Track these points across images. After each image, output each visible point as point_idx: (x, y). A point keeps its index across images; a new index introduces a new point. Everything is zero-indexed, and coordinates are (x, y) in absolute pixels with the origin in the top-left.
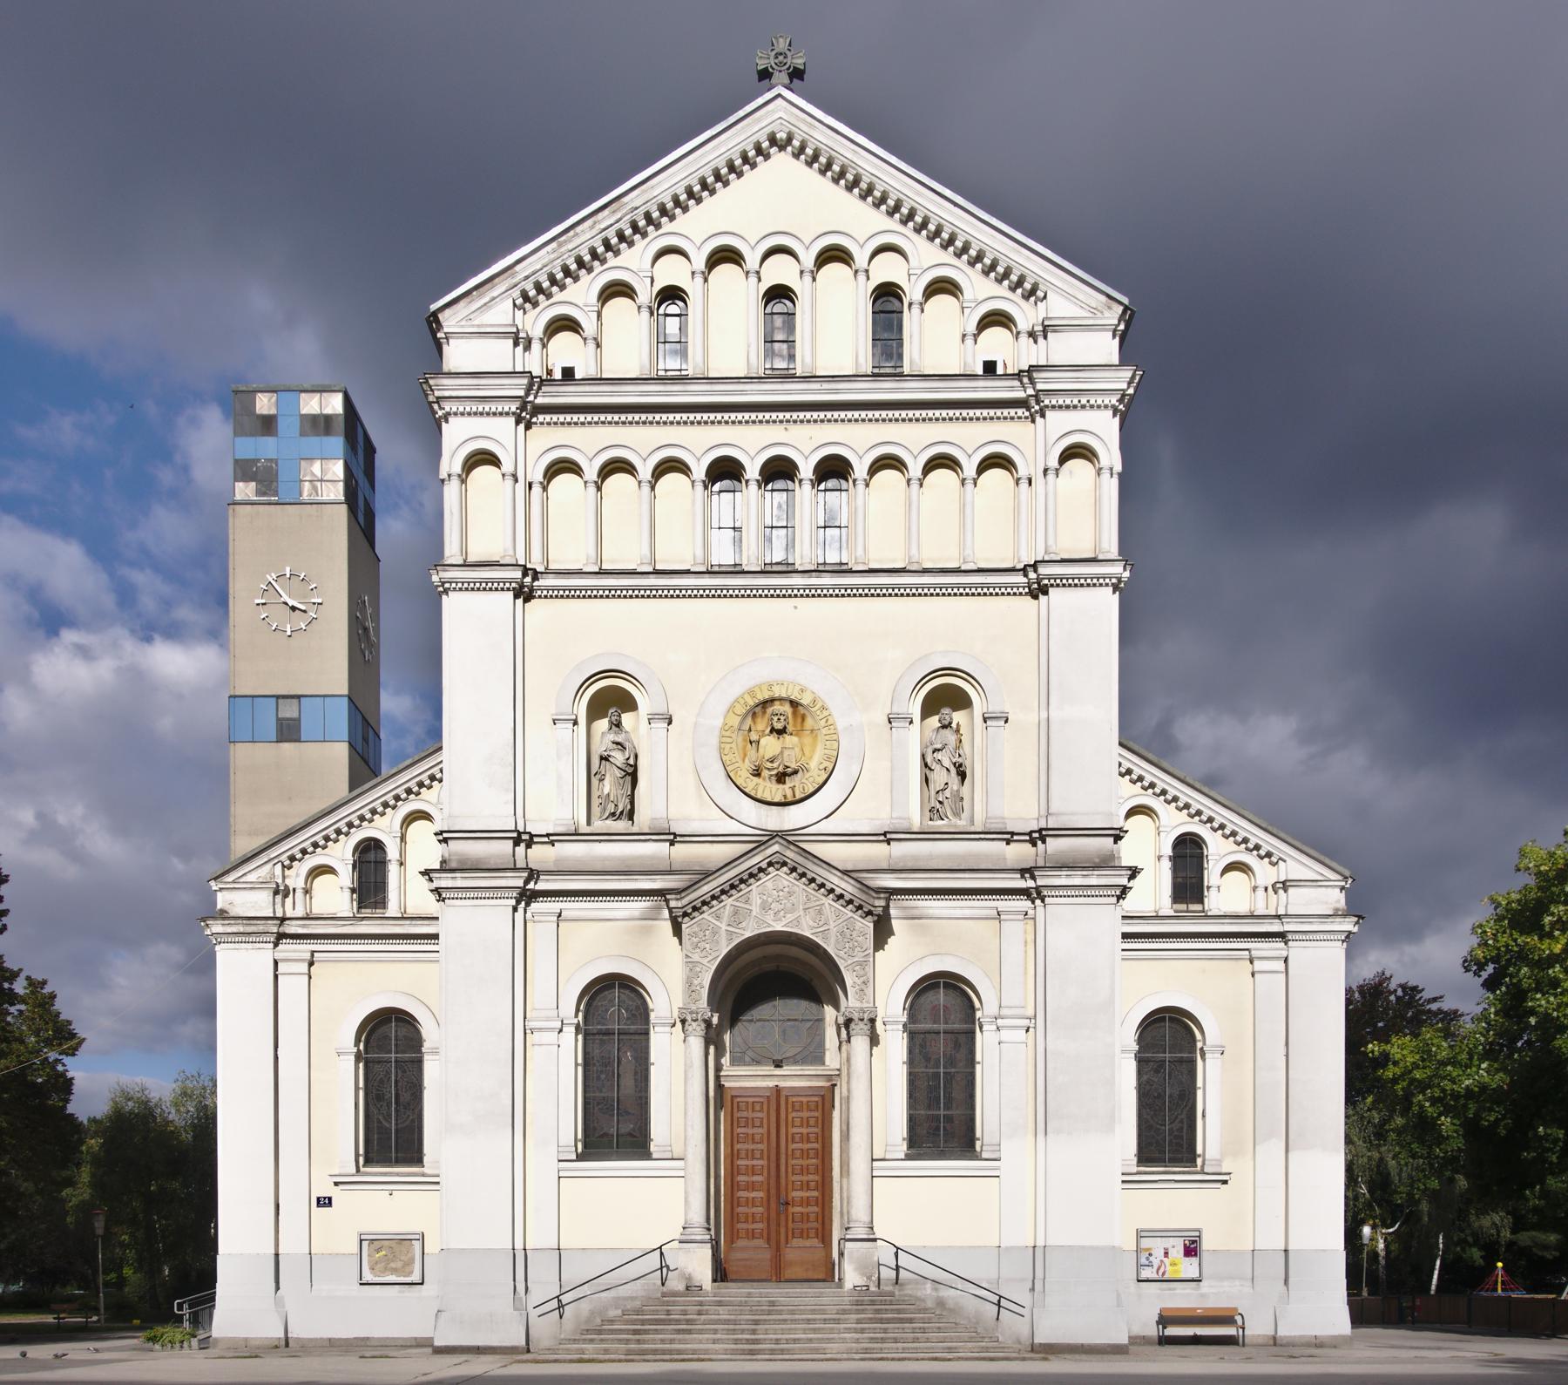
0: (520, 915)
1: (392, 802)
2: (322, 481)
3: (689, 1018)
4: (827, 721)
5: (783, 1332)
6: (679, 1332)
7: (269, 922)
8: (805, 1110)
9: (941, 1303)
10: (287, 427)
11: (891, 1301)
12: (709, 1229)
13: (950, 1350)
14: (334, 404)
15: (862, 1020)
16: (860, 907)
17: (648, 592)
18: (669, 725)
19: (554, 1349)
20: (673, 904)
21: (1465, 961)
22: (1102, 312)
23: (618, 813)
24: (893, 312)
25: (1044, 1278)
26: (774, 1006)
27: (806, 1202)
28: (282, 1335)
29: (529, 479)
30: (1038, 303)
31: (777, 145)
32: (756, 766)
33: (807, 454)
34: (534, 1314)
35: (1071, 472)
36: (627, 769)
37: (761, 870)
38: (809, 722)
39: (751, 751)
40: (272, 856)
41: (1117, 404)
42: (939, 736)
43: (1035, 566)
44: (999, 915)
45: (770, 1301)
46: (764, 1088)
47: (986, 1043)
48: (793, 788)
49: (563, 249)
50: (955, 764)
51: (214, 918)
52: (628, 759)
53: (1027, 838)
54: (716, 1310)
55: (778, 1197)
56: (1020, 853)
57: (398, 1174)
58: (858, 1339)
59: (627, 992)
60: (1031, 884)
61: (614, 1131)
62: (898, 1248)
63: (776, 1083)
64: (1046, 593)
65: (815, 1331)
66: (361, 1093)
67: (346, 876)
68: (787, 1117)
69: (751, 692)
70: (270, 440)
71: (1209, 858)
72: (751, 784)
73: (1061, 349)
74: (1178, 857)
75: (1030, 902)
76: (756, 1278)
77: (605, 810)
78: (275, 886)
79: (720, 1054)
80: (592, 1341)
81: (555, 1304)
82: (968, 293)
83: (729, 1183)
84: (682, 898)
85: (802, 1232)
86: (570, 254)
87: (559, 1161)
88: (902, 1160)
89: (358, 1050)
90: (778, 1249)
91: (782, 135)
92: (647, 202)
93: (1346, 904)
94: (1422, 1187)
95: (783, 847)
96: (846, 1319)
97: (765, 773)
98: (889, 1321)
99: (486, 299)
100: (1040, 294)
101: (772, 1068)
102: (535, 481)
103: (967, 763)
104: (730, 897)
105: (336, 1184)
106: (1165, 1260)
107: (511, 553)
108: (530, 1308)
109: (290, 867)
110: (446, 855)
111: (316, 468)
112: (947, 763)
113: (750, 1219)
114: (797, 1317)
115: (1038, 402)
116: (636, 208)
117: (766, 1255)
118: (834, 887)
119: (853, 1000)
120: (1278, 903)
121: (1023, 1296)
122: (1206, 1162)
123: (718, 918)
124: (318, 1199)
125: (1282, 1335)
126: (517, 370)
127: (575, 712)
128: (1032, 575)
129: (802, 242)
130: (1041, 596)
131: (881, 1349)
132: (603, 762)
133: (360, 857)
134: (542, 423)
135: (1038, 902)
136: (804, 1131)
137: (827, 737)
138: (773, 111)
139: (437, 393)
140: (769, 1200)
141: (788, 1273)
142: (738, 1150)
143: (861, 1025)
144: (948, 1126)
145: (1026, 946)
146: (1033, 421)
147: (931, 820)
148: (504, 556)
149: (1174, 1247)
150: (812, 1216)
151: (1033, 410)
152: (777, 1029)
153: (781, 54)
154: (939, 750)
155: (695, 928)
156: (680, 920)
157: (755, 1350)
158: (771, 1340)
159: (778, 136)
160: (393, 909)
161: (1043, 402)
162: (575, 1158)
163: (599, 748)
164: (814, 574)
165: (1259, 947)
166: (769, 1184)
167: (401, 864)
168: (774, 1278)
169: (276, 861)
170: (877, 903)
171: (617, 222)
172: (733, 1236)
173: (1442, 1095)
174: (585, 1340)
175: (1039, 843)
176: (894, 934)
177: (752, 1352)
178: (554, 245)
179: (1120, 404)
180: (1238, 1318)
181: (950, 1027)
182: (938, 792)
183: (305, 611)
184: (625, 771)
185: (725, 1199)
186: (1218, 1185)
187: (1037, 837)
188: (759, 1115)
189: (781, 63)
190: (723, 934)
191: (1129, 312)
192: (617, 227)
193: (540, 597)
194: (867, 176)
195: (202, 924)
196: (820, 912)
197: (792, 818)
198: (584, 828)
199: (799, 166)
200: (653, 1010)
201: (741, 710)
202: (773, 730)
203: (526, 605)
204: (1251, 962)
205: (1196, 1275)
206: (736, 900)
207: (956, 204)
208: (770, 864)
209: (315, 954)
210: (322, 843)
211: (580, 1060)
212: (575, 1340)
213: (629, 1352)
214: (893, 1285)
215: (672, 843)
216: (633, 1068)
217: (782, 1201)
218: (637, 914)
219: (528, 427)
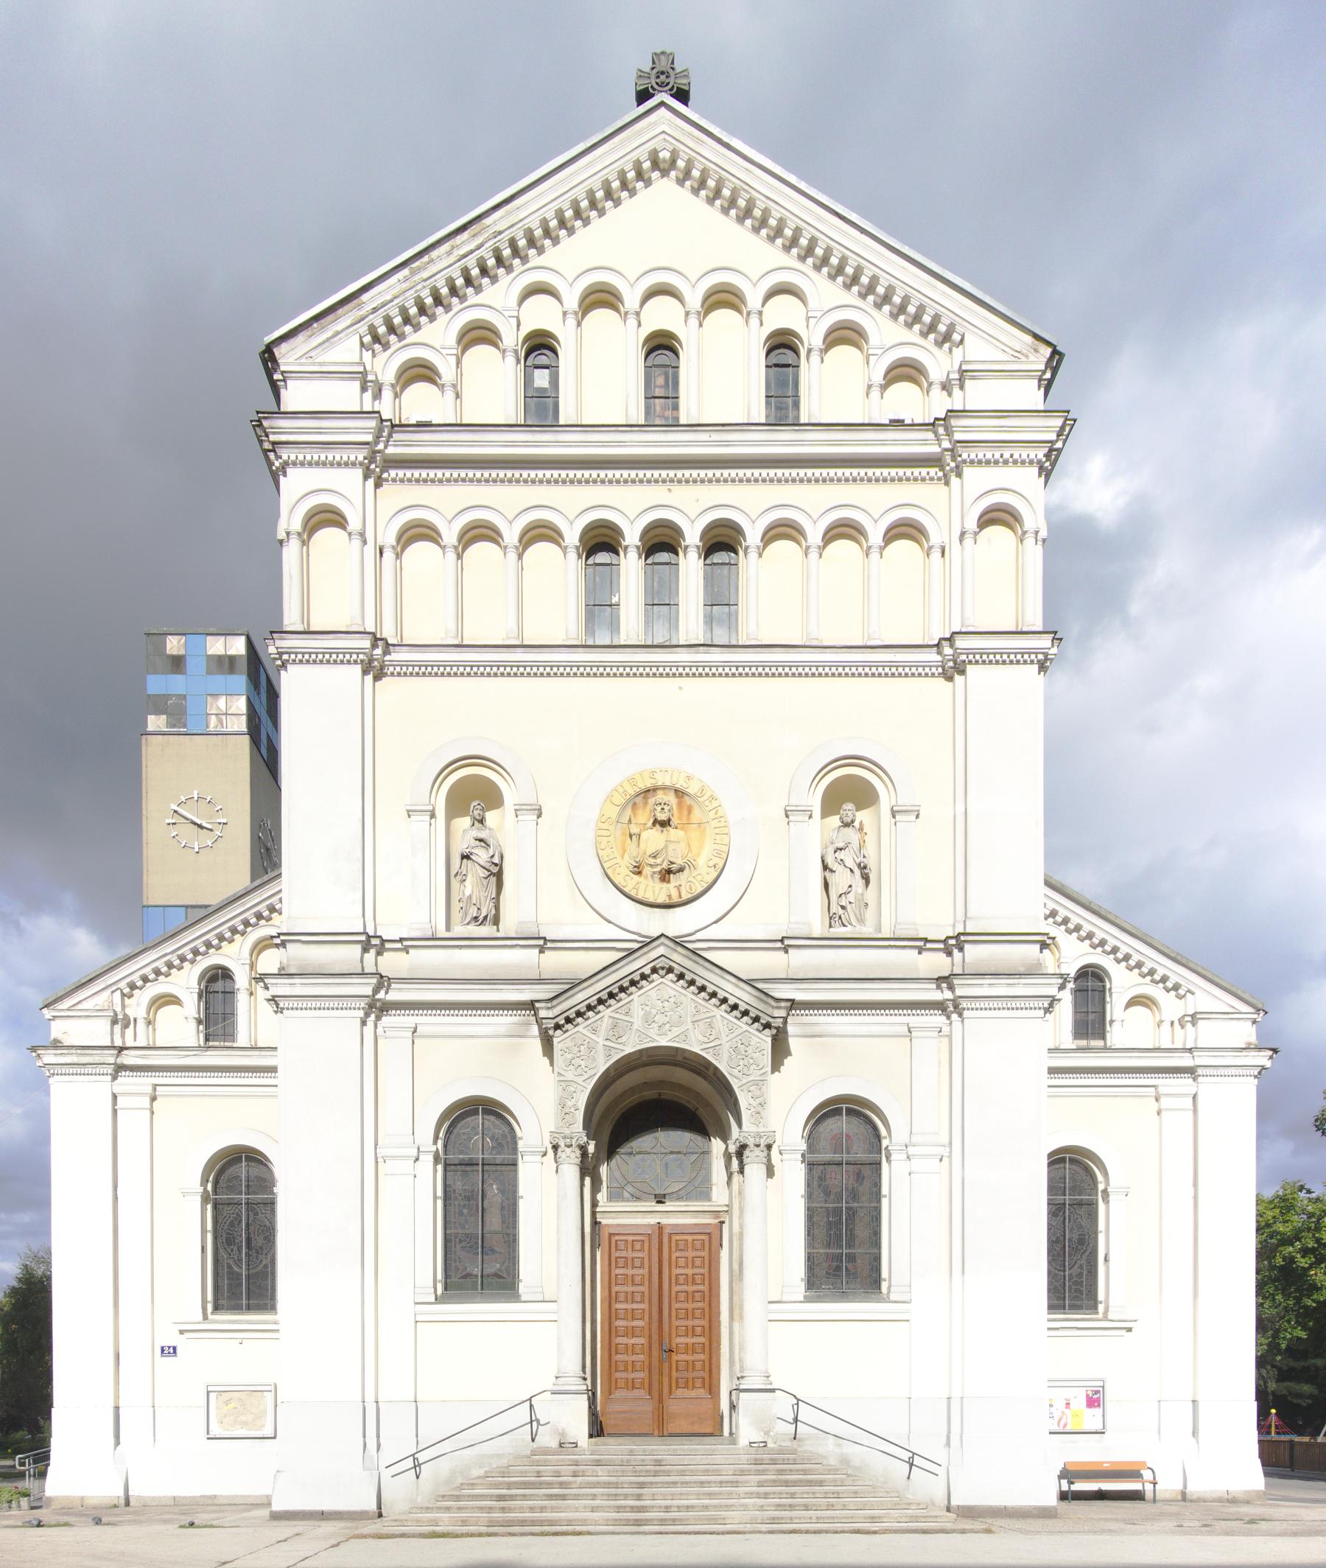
0: (369, 1028)
1: (241, 928)
2: (226, 714)
3: (562, 1143)
4: (716, 813)
5: (673, 1496)
6: (550, 1497)
7: (106, 1052)
8: (690, 1249)
9: (845, 1461)
10: (195, 666)
11: (795, 1459)
12: (585, 1379)
13: (873, 1519)
14: (238, 646)
15: (758, 1146)
16: (756, 1019)
17: (515, 669)
18: (538, 818)
19: (401, 1521)
20: (542, 1014)
21: (1316, 1120)
22: (1027, 356)
23: (481, 918)
24: (788, 366)
25: (962, 1433)
26: (656, 1138)
27: (692, 1349)
28: (121, 1493)
29: (380, 542)
30: (954, 348)
31: (659, 169)
32: (637, 862)
33: (693, 518)
34: (386, 1474)
35: (989, 540)
36: (491, 868)
37: (644, 977)
38: (697, 815)
39: (631, 846)
40: (110, 982)
41: (1044, 459)
42: (840, 834)
43: (950, 640)
44: (910, 1032)
45: (656, 1460)
46: (645, 1225)
47: (894, 1176)
49: (417, 278)
50: (859, 865)
51: (45, 1047)
52: (492, 856)
53: (942, 946)
54: (593, 1471)
55: (661, 1342)
56: (936, 963)
57: (248, 1322)
58: (762, 1506)
59: (492, 1118)
60: (948, 995)
61: (477, 1271)
62: (798, 1400)
63: (659, 1221)
64: (962, 672)
65: (710, 1495)
66: (210, 1237)
67: (191, 1005)
68: (670, 1257)
69: (631, 780)
70: (179, 678)
71: (1113, 991)
72: (631, 883)
73: (978, 395)
74: (1079, 991)
75: (945, 1018)
76: (637, 1432)
77: (466, 914)
78: (112, 1014)
79: (596, 1188)
80: (448, 1509)
81: (410, 1463)
82: (874, 339)
83: (607, 1329)
84: (554, 1007)
85: (687, 1382)
86: (425, 284)
87: (416, 1303)
88: (800, 1302)
89: (205, 1190)
90: (661, 1400)
91: (664, 155)
92: (512, 226)
93: (1257, 1039)
94: (1289, 1336)
95: (668, 949)
96: (745, 1482)
97: (647, 871)
98: (795, 1483)
99: (329, 334)
100: (956, 337)
101: (654, 1204)
102: (388, 545)
103: (872, 864)
104: (608, 1007)
105: (182, 1332)
106: (1067, 1411)
107: (360, 622)
108: (382, 1465)
109: (130, 996)
110: (285, 962)
111: (222, 702)
112: (850, 863)
113: (630, 1368)
114: (687, 1478)
115: (953, 458)
116: (500, 233)
117: (648, 1407)
118: (727, 996)
119: (749, 1124)
120: (1187, 1036)
121: (939, 1454)
122: (1110, 1309)
123: (594, 1031)
125: (1192, 1490)
126: (364, 410)
127: (433, 802)
128: (948, 651)
129: (688, 280)
130: (957, 677)
131: (791, 1518)
132: (465, 860)
133: (207, 987)
134: (394, 480)
135: (954, 1017)
136: (690, 1271)
137: (717, 831)
138: (655, 123)
139: (272, 438)
140: (650, 1347)
141: (672, 1428)
142: (616, 1292)
143: (757, 1151)
144: (850, 1266)
145: (939, 1066)
146: (947, 483)
147: (830, 926)
148: (351, 625)
149: (1075, 1397)
150: (698, 1365)
151: (948, 468)
152: (658, 1162)
153: (663, 73)
154: (841, 849)
155: (569, 1043)
156: (551, 1032)
157: (642, 1520)
158: (660, 1507)
159: (661, 155)
160: (242, 1040)
161: (960, 456)
162: (434, 1300)
163: (460, 846)
164: (702, 648)
165: (1167, 1084)
166: (650, 1329)
167: (251, 994)
168: (656, 1433)
169: (114, 988)
170: (777, 1013)
171: (478, 248)
172: (610, 1386)
173: (1316, 1246)
174: (439, 1508)
175: (955, 951)
176: (791, 1055)
177: (638, 1523)
178: (406, 272)
179: (1047, 461)
180: (1147, 1475)
181: (851, 1157)
182: (840, 896)
183: (211, 830)
184: (488, 871)
185: (602, 1346)
186: (1123, 1332)
187: (952, 945)
188: (640, 1255)
189: (663, 83)
190: (600, 1048)
191: (1057, 357)
192: (477, 254)
193: (392, 674)
194: (763, 202)
195: (34, 1054)
196: (710, 1025)
197: (677, 922)
198: (442, 932)
199: (684, 194)
200: (521, 1138)
201: (620, 800)
202: (655, 822)
203: (376, 683)
204: (1157, 1100)
205: (1099, 1427)
206: (616, 1011)
207: (863, 231)
208: (654, 970)
209: (157, 1088)
210: (164, 969)
211: (440, 1193)
212: (428, 1508)
213: (491, 1524)
214: (790, 1440)
215: (542, 950)
216: (500, 1201)
217: (664, 1348)
218: (502, 1030)
219: (378, 485)
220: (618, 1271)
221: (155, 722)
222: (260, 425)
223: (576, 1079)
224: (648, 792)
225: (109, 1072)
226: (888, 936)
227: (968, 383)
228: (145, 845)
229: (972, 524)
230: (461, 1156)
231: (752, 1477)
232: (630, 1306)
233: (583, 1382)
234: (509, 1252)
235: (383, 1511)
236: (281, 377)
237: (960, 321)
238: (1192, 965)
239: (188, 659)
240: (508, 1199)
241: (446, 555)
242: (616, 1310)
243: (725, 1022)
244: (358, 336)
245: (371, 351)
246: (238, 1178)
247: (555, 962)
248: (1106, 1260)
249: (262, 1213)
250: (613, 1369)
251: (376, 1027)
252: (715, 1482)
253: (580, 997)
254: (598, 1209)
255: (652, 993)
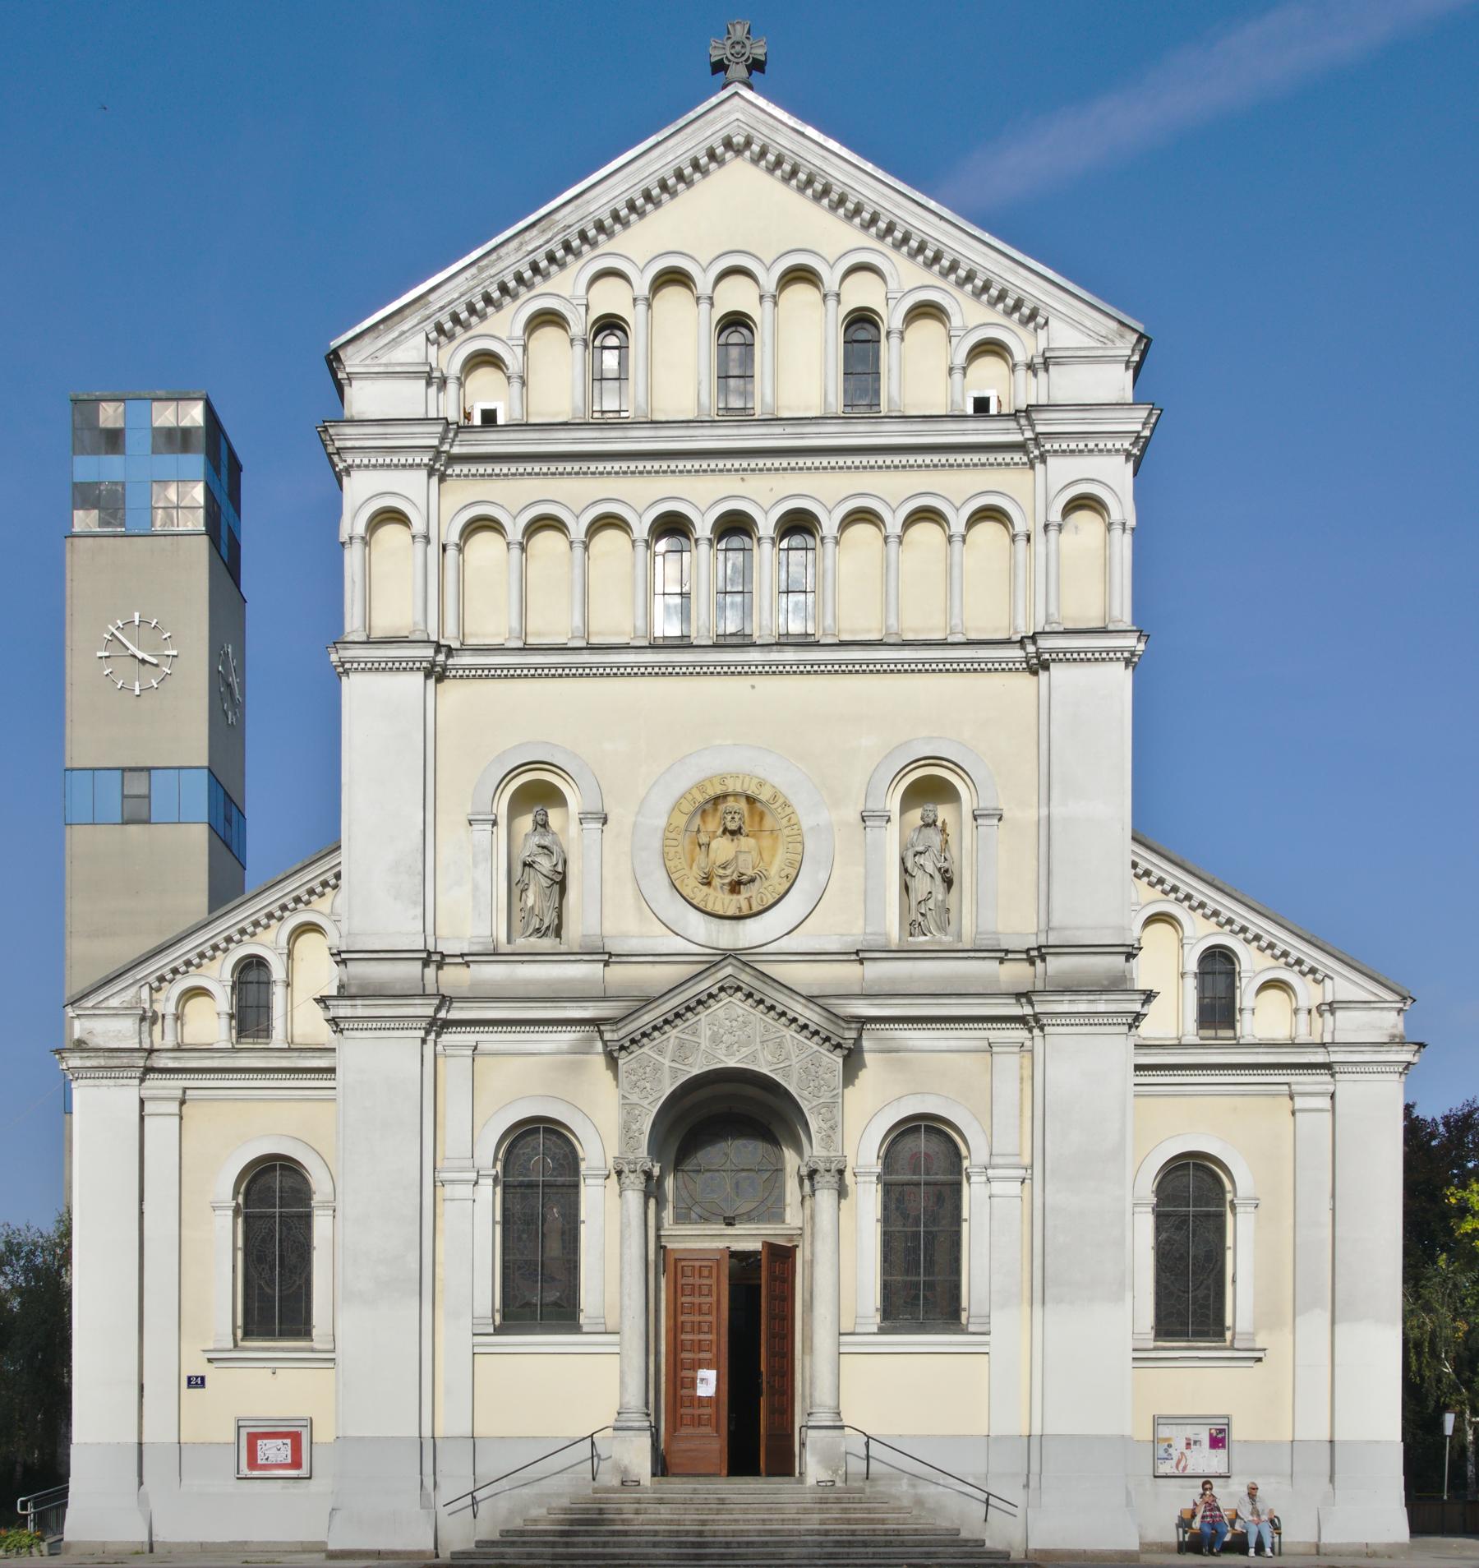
2: (178, 507)
3: (626, 1169)
4: (789, 820)
7: (136, 1054)
9: (919, 1502)
10: (139, 443)
11: (860, 1498)
12: (648, 1415)
14: (194, 415)
15: (829, 1171)
18: (603, 825)
20: (608, 1036)
22: (1113, 342)
23: (543, 928)
28: (146, 1538)
29: (443, 540)
34: (443, 1512)
35: (1076, 528)
36: (554, 877)
38: (768, 823)
39: (700, 856)
42: (921, 837)
43: (1033, 638)
45: (719, 1499)
47: (973, 1195)
48: (749, 899)
49: (484, 275)
50: (940, 869)
56: (1015, 973)
59: (554, 1138)
60: (1027, 1010)
62: (869, 1437)
66: (240, 1255)
67: (223, 1000)
69: (700, 787)
70: (116, 459)
72: (700, 894)
75: (1027, 1032)
77: (528, 924)
79: (660, 1205)
82: (956, 321)
84: (620, 1029)
86: (492, 280)
87: (474, 1335)
88: (874, 1334)
91: (739, 140)
97: (716, 882)
100: (1040, 320)
101: (724, 1226)
104: (674, 1028)
105: (210, 1360)
109: (159, 989)
110: (345, 979)
111: (172, 493)
112: (930, 868)
116: (569, 227)
120: (1323, 1028)
122: (1237, 1337)
123: (661, 1052)
124: (189, 1379)
126: (429, 417)
127: (495, 811)
132: (527, 869)
135: (1036, 1032)
137: (789, 839)
138: (729, 112)
139: (338, 444)
142: (682, 1322)
143: (828, 1177)
153: (738, 43)
154: (921, 853)
159: (735, 140)
160: (278, 1038)
164: (775, 648)
165: (1303, 1081)
167: (288, 985)
170: (848, 1034)
171: (547, 242)
175: (1038, 961)
178: (473, 270)
183: (156, 665)
184: (552, 880)
186: (1251, 1364)
187: (1036, 955)
189: (738, 54)
191: (1145, 340)
195: (57, 1056)
196: (780, 1046)
197: (750, 933)
200: (584, 1159)
201: (688, 807)
206: (682, 1031)
208: (722, 989)
211: (498, 1218)
215: (606, 964)
216: (560, 1226)
218: (565, 1047)
219: (443, 478)
220: (684, 1299)
221: (84, 520)
222: (326, 430)
223: (641, 1102)
224: (718, 800)
225: (138, 1075)
226: (969, 948)
227: (1051, 368)
228: (68, 686)
229: (1056, 516)
230: (520, 1179)
231: (815, 1515)
232: (696, 1337)
233: (646, 1418)
234: (570, 1281)
235: (439, 1551)
236: (345, 376)
237: (1044, 305)
238: (1328, 948)
239: (128, 434)
240: (569, 1223)
241: (511, 551)
242: (682, 1341)
243: (796, 1041)
244: (424, 334)
245: (436, 346)
246: (271, 1189)
247: (618, 974)
248: (1234, 1281)
249: (296, 1228)
250: (679, 1405)
251: (435, 1043)
252: (777, 1520)
253: (647, 1019)
254: (662, 1233)
255: (721, 1013)
